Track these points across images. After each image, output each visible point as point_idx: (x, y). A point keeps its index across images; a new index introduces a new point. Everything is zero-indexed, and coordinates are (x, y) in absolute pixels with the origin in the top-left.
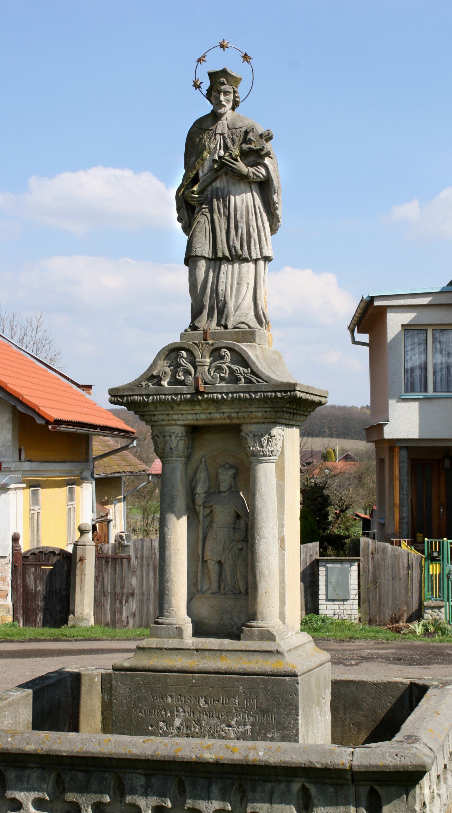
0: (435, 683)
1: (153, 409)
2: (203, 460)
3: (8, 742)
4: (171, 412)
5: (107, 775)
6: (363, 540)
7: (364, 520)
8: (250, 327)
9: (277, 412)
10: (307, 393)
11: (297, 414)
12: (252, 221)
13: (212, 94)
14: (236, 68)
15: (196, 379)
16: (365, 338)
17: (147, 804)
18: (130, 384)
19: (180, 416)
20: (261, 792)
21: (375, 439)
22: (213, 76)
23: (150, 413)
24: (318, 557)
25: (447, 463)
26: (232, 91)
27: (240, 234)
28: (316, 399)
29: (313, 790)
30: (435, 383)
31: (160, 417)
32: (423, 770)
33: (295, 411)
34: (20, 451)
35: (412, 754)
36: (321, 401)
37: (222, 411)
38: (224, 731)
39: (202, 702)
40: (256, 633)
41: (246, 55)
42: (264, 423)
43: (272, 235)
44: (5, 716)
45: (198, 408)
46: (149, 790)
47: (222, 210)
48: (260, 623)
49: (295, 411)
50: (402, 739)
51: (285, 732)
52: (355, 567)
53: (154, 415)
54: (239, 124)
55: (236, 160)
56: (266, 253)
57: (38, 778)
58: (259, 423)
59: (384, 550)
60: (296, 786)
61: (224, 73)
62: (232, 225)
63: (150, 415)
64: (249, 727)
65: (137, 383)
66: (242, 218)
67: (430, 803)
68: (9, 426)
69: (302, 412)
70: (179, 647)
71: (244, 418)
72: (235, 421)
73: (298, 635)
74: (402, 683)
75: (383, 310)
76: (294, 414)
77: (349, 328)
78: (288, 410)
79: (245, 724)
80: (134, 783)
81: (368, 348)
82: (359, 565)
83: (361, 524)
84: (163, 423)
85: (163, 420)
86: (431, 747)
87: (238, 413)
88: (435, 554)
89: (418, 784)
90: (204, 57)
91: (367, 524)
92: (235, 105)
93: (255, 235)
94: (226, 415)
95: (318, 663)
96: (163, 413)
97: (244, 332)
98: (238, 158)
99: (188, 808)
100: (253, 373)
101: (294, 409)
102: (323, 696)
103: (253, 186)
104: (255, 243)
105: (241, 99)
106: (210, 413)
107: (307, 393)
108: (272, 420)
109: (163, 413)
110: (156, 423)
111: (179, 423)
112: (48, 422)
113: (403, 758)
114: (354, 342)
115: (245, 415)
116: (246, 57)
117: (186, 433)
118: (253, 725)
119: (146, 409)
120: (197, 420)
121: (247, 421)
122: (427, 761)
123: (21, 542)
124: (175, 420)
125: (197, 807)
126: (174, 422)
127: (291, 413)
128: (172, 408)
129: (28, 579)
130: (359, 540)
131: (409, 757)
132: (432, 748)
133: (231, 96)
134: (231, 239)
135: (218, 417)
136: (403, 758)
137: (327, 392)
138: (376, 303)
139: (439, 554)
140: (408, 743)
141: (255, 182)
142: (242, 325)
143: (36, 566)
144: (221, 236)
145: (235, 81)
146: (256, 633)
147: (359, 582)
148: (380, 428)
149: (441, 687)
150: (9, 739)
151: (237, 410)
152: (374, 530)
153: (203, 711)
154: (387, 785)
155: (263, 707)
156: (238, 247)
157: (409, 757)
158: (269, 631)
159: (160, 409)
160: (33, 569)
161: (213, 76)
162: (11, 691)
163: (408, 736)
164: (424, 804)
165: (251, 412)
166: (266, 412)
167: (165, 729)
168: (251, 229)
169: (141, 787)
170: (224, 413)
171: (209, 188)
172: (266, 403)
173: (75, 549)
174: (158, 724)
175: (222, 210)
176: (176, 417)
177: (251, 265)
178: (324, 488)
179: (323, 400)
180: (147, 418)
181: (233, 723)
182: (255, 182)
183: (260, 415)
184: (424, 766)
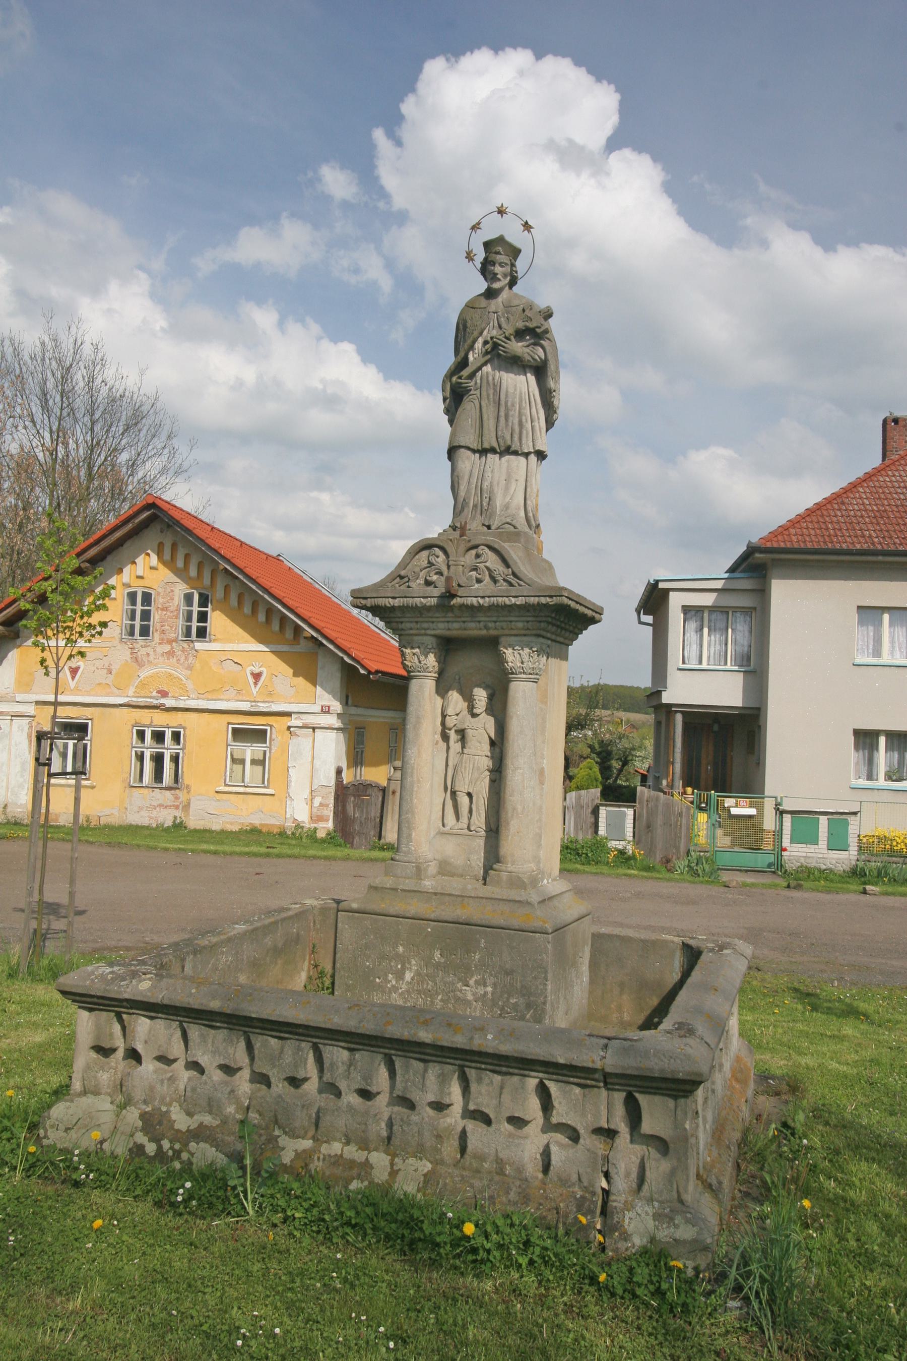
0: (711, 945)
1: (399, 615)
2: (457, 677)
3: (191, 994)
4: (419, 619)
5: (303, 1044)
6: (639, 788)
7: (643, 775)
8: (515, 527)
9: (540, 622)
10: (577, 603)
11: (566, 630)
12: (525, 408)
13: (486, 269)
14: (515, 235)
15: (448, 579)
16: (649, 619)
17: (348, 1086)
18: (375, 584)
19: (431, 624)
20: (488, 1085)
21: (655, 704)
22: (487, 245)
23: (397, 620)
24: (599, 802)
25: (716, 728)
26: (509, 262)
27: (510, 424)
28: (589, 613)
29: (553, 1087)
30: (709, 657)
31: (408, 625)
32: (698, 1079)
33: (563, 625)
34: (347, 697)
35: (685, 1055)
36: (594, 617)
37: (477, 619)
38: (461, 991)
39: (437, 954)
40: (504, 878)
41: (526, 223)
42: (525, 635)
43: (547, 430)
44: (223, 953)
45: (450, 615)
46: (352, 1068)
47: (491, 396)
48: (510, 867)
49: (563, 625)
50: (671, 1028)
51: (532, 999)
52: (630, 812)
53: (402, 622)
54: (516, 302)
55: (509, 339)
56: (540, 447)
57: (225, 1040)
58: (520, 635)
59: (657, 799)
60: (532, 1082)
61: (501, 240)
62: (502, 413)
63: (397, 622)
64: (489, 989)
65: (381, 584)
66: (513, 405)
67: (703, 1110)
68: (339, 675)
69: (571, 628)
70: (416, 889)
71: (502, 628)
72: (493, 632)
73: (555, 883)
74: (673, 942)
75: (667, 591)
76: (562, 628)
77: (636, 610)
78: (554, 622)
79: (485, 985)
80: (335, 1057)
81: (651, 628)
82: (635, 811)
83: (639, 778)
84: (411, 632)
85: (411, 629)
86: (708, 1041)
87: (495, 622)
88: (703, 805)
89: (539, 56)
90: (479, 223)
91: (644, 779)
92: (513, 282)
93: (528, 426)
94: (482, 624)
95: (576, 916)
96: (411, 620)
97: (509, 533)
98: (512, 337)
99: (398, 1096)
100: (514, 574)
101: (562, 622)
102: (580, 955)
103: (527, 370)
104: (527, 434)
105: (520, 276)
106: (464, 622)
107: (577, 603)
108: (534, 632)
109: (411, 620)
110: (403, 632)
111: (429, 632)
112: (370, 672)
113: (672, 1060)
114: (640, 622)
115: (504, 624)
116: (527, 226)
117: (438, 645)
118: (495, 986)
119: (392, 615)
120: (449, 629)
121: (507, 632)
122: (705, 1069)
123: (344, 775)
124: (425, 629)
125: (408, 1096)
126: (423, 632)
127: (558, 626)
128: (421, 614)
129: (348, 807)
130: (635, 788)
131: (681, 1060)
132: (710, 1043)
133: (508, 269)
134: (500, 428)
135: (474, 629)
136: (672, 1060)
137: (602, 609)
138: (661, 585)
139: (707, 805)
140: (680, 1037)
141: (531, 367)
142: (507, 526)
143: (355, 796)
144: (490, 424)
145: (515, 252)
146: (504, 878)
147: (634, 828)
148: (659, 693)
149: (718, 951)
150: (193, 991)
151: (494, 619)
152: (650, 782)
153: (438, 965)
154: (650, 1093)
155: (507, 966)
156: (508, 437)
157: (681, 1060)
158: (519, 878)
159: (408, 615)
160: (352, 799)
161: (487, 245)
162: (237, 924)
163: (679, 1023)
164: (697, 1113)
165: (511, 622)
166: (528, 622)
167: (394, 982)
168: (524, 418)
169: (342, 1063)
170: (479, 622)
171: (479, 374)
172: (528, 611)
173: (388, 784)
174: (387, 976)
175: (491, 396)
176: (425, 625)
177: (522, 459)
178: (609, 745)
179: (597, 616)
180: (394, 625)
181: (472, 982)
182: (531, 367)
183: (520, 625)
184: (701, 1075)
